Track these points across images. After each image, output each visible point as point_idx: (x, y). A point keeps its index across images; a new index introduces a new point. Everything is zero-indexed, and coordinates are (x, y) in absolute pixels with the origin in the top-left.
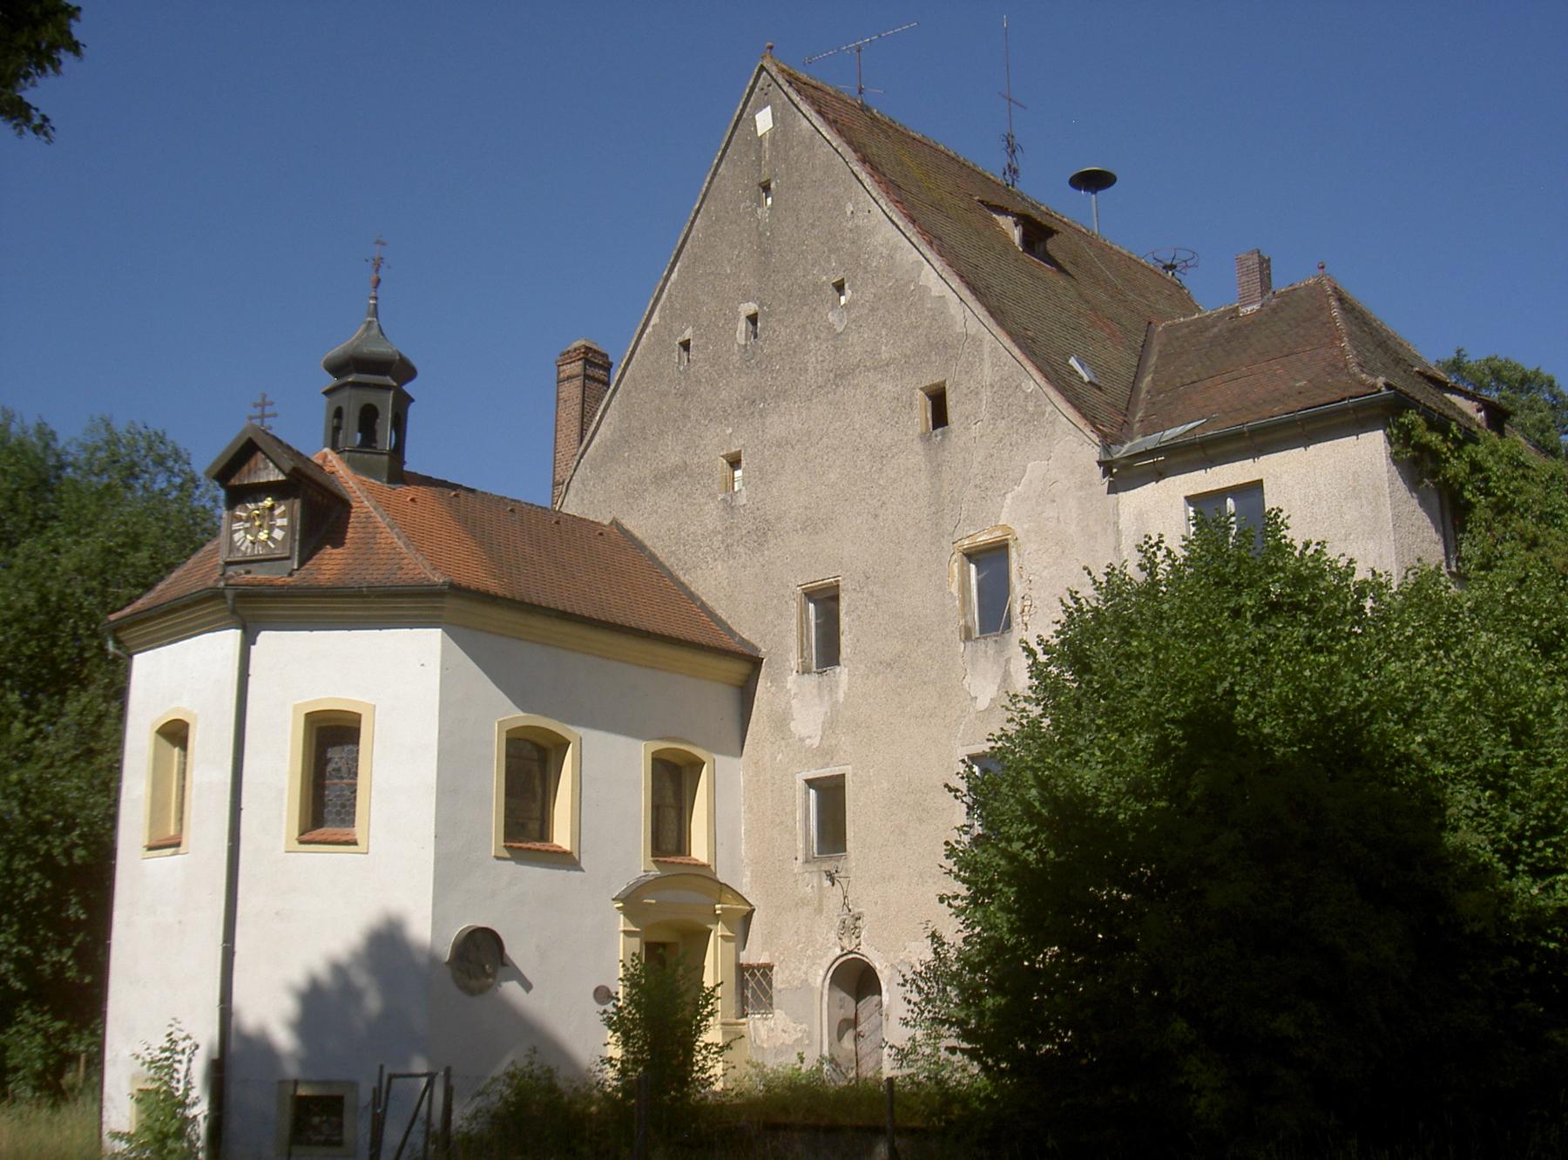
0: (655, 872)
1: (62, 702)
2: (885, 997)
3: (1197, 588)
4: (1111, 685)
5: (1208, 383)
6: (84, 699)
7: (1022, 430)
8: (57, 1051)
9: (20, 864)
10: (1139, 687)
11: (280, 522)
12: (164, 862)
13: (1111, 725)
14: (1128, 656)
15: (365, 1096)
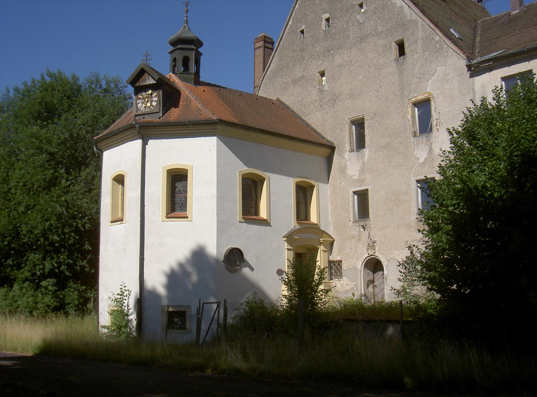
0: (298, 227)
1: (80, 173)
2: (385, 272)
5: (504, 37)
6: (87, 170)
8: (83, 297)
9: (67, 230)
11: (154, 99)
12: (117, 226)
15: (194, 311)
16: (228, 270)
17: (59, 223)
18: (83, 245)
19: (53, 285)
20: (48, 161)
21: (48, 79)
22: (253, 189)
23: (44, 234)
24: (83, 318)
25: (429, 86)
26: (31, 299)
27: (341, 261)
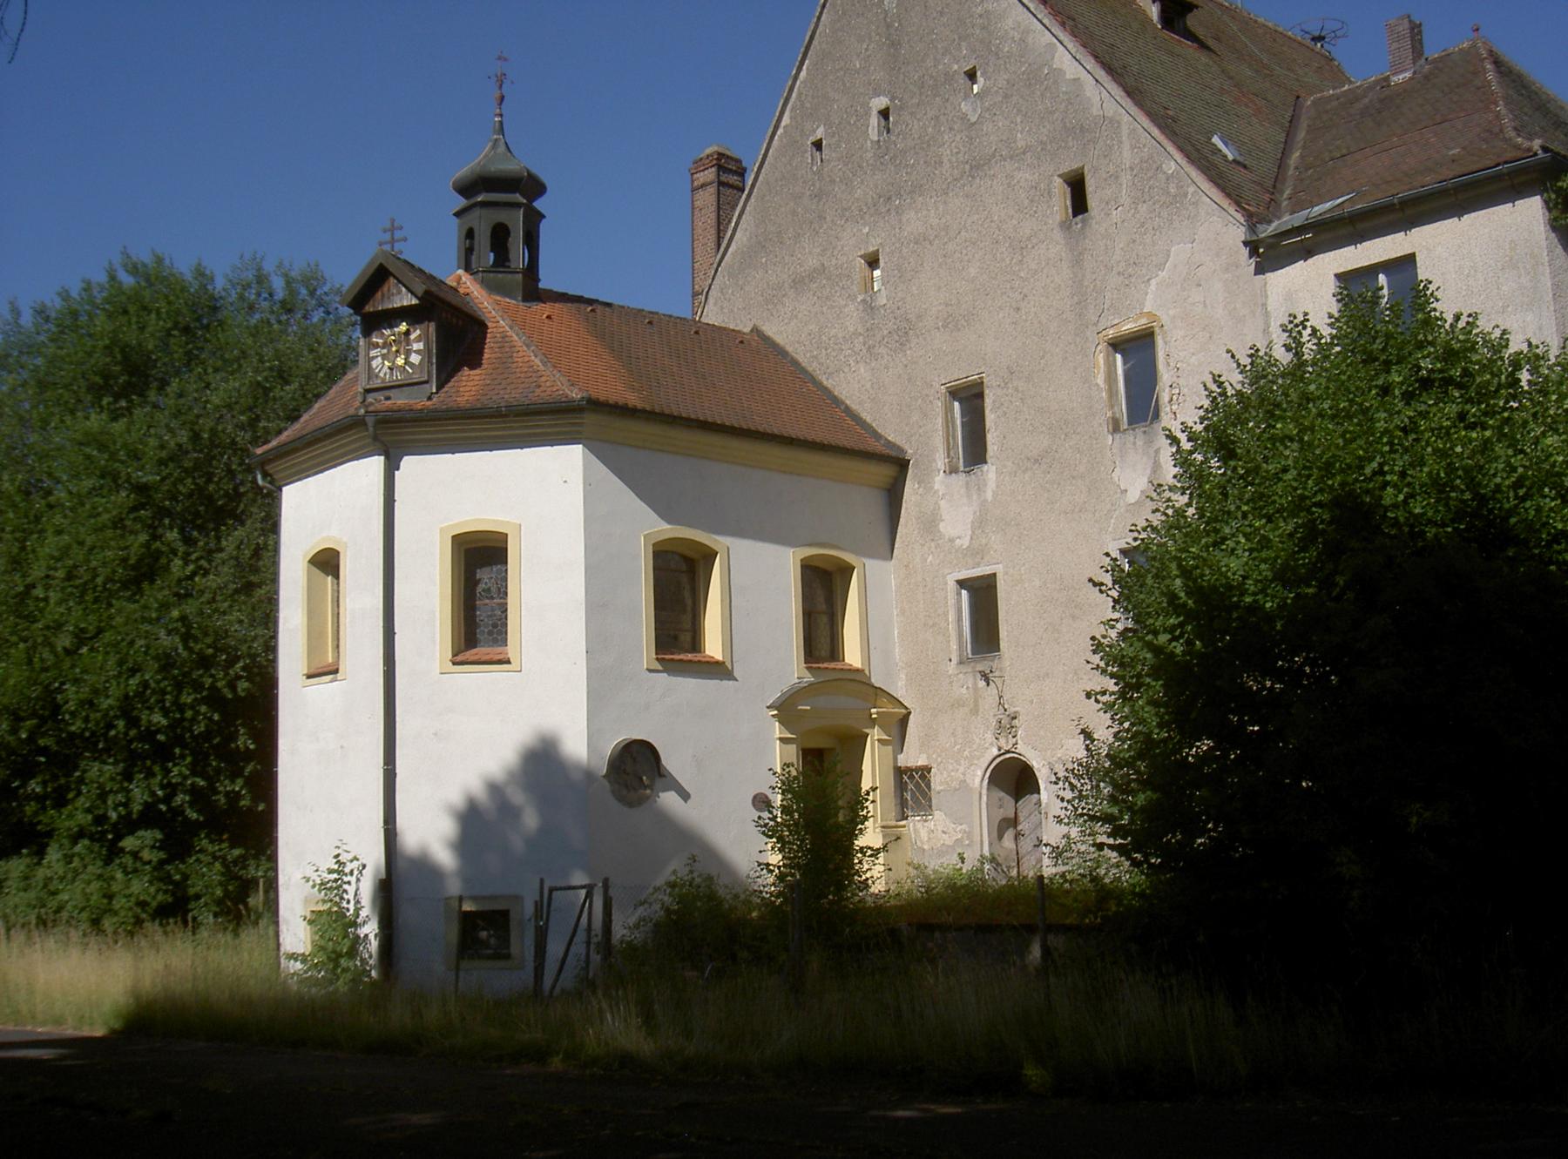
0: (809, 678)
1: (218, 539)
2: (1044, 795)
3: (1343, 367)
4: (1257, 469)
5: (1358, 156)
7: (1165, 214)
9: (187, 698)
10: (1285, 470)
11: (416, 346)
13: (1257, 511)
14: (1273, 439)
15: (529, 909)
16: (621, 799)
17: (164, 679)
18: (233, 737)
19: (153, 847)
20: (134, 509)
21: (127, 280)
22: (684, 579)
23: (127, 709)
24: (236, 934)
25: (1150, 297)
26: (95, 886)
27: (929, 770)
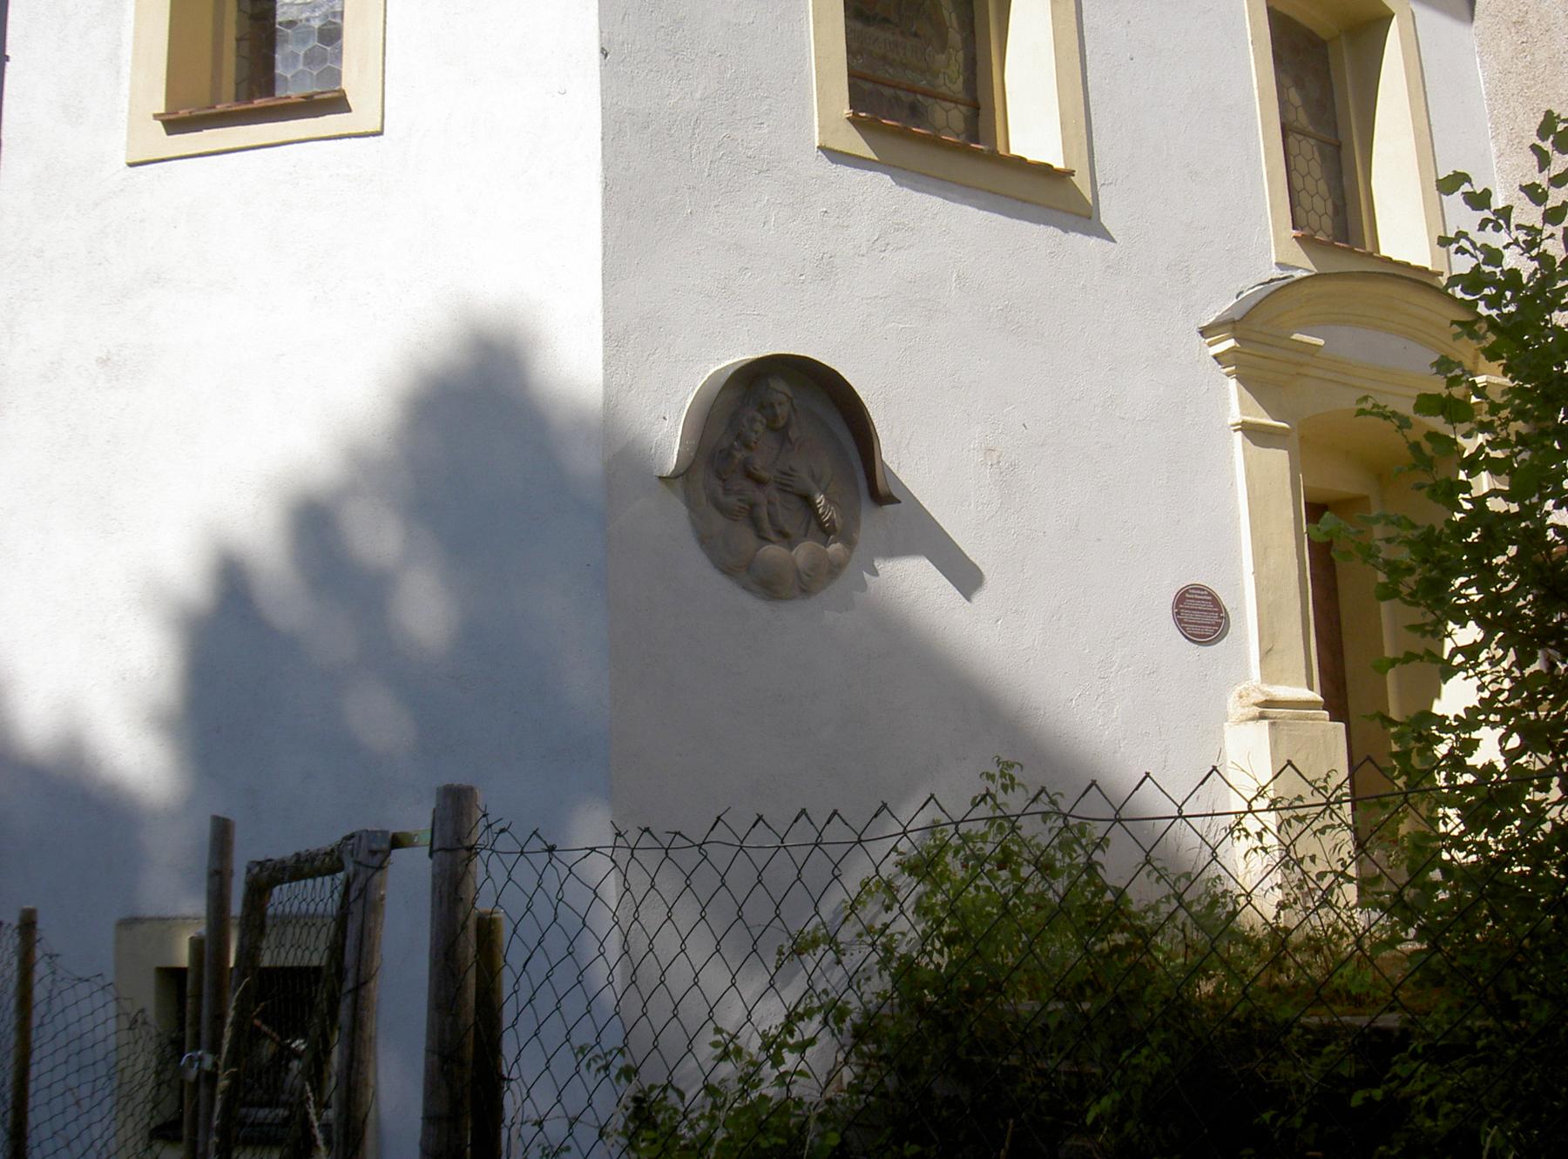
16: (737, 568)
